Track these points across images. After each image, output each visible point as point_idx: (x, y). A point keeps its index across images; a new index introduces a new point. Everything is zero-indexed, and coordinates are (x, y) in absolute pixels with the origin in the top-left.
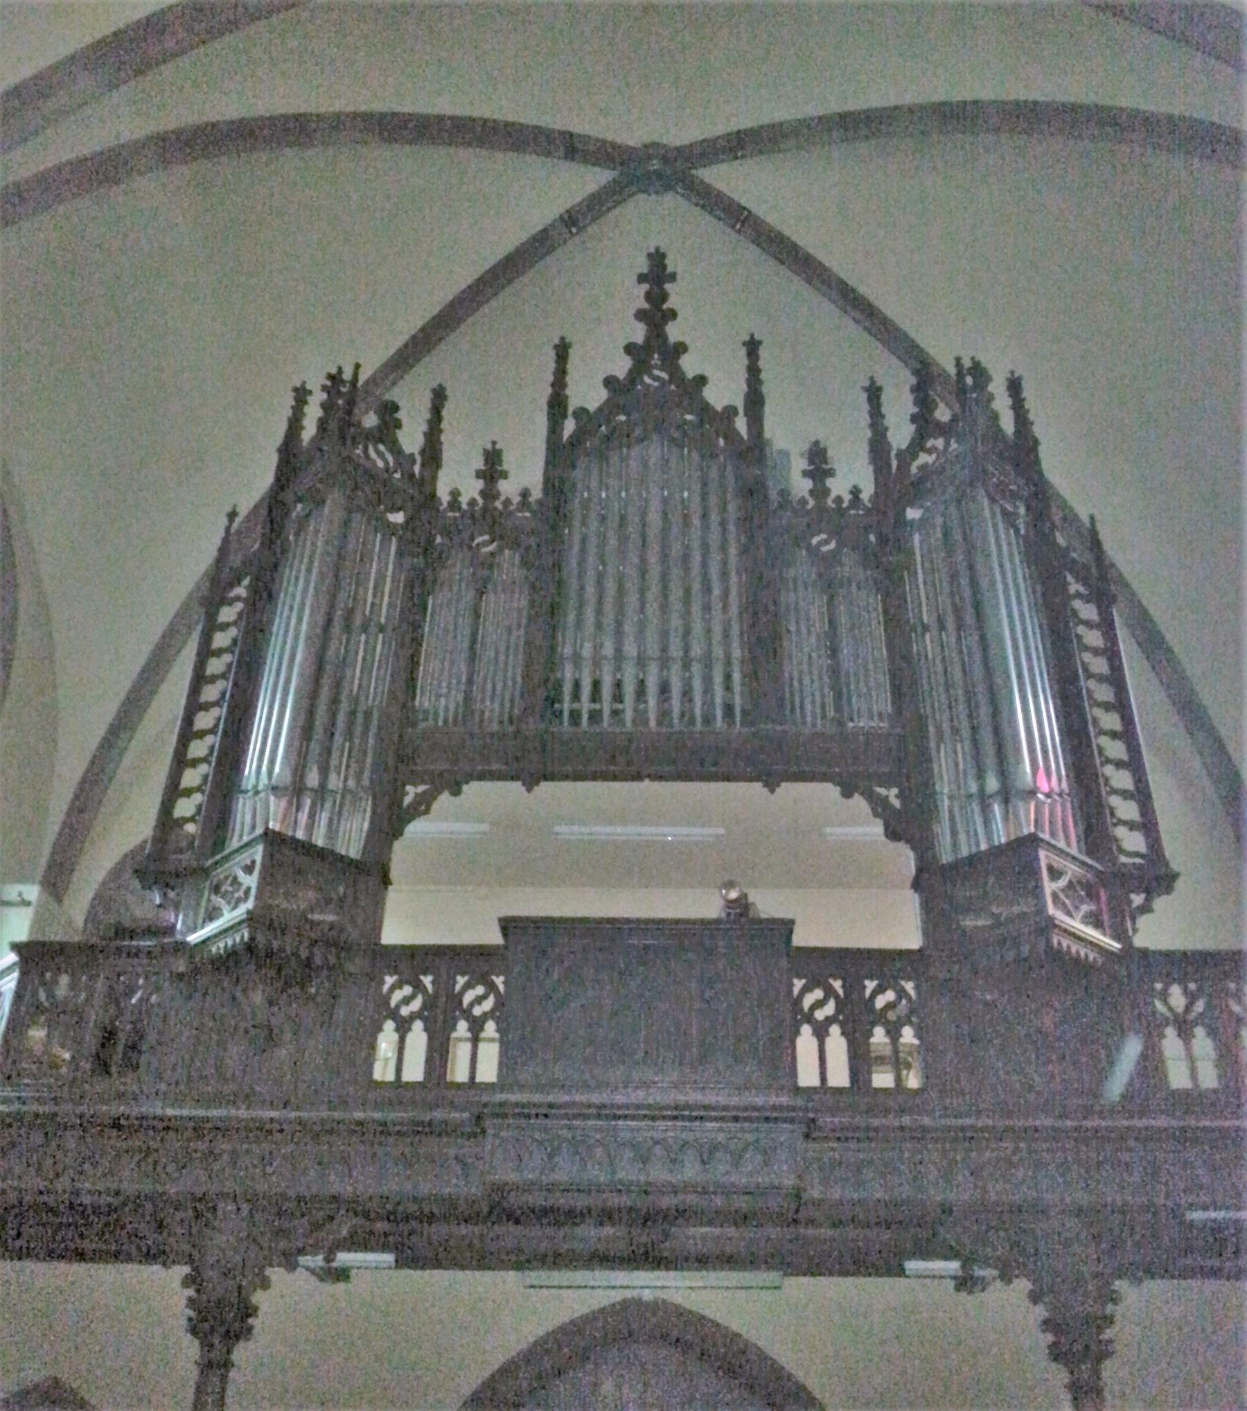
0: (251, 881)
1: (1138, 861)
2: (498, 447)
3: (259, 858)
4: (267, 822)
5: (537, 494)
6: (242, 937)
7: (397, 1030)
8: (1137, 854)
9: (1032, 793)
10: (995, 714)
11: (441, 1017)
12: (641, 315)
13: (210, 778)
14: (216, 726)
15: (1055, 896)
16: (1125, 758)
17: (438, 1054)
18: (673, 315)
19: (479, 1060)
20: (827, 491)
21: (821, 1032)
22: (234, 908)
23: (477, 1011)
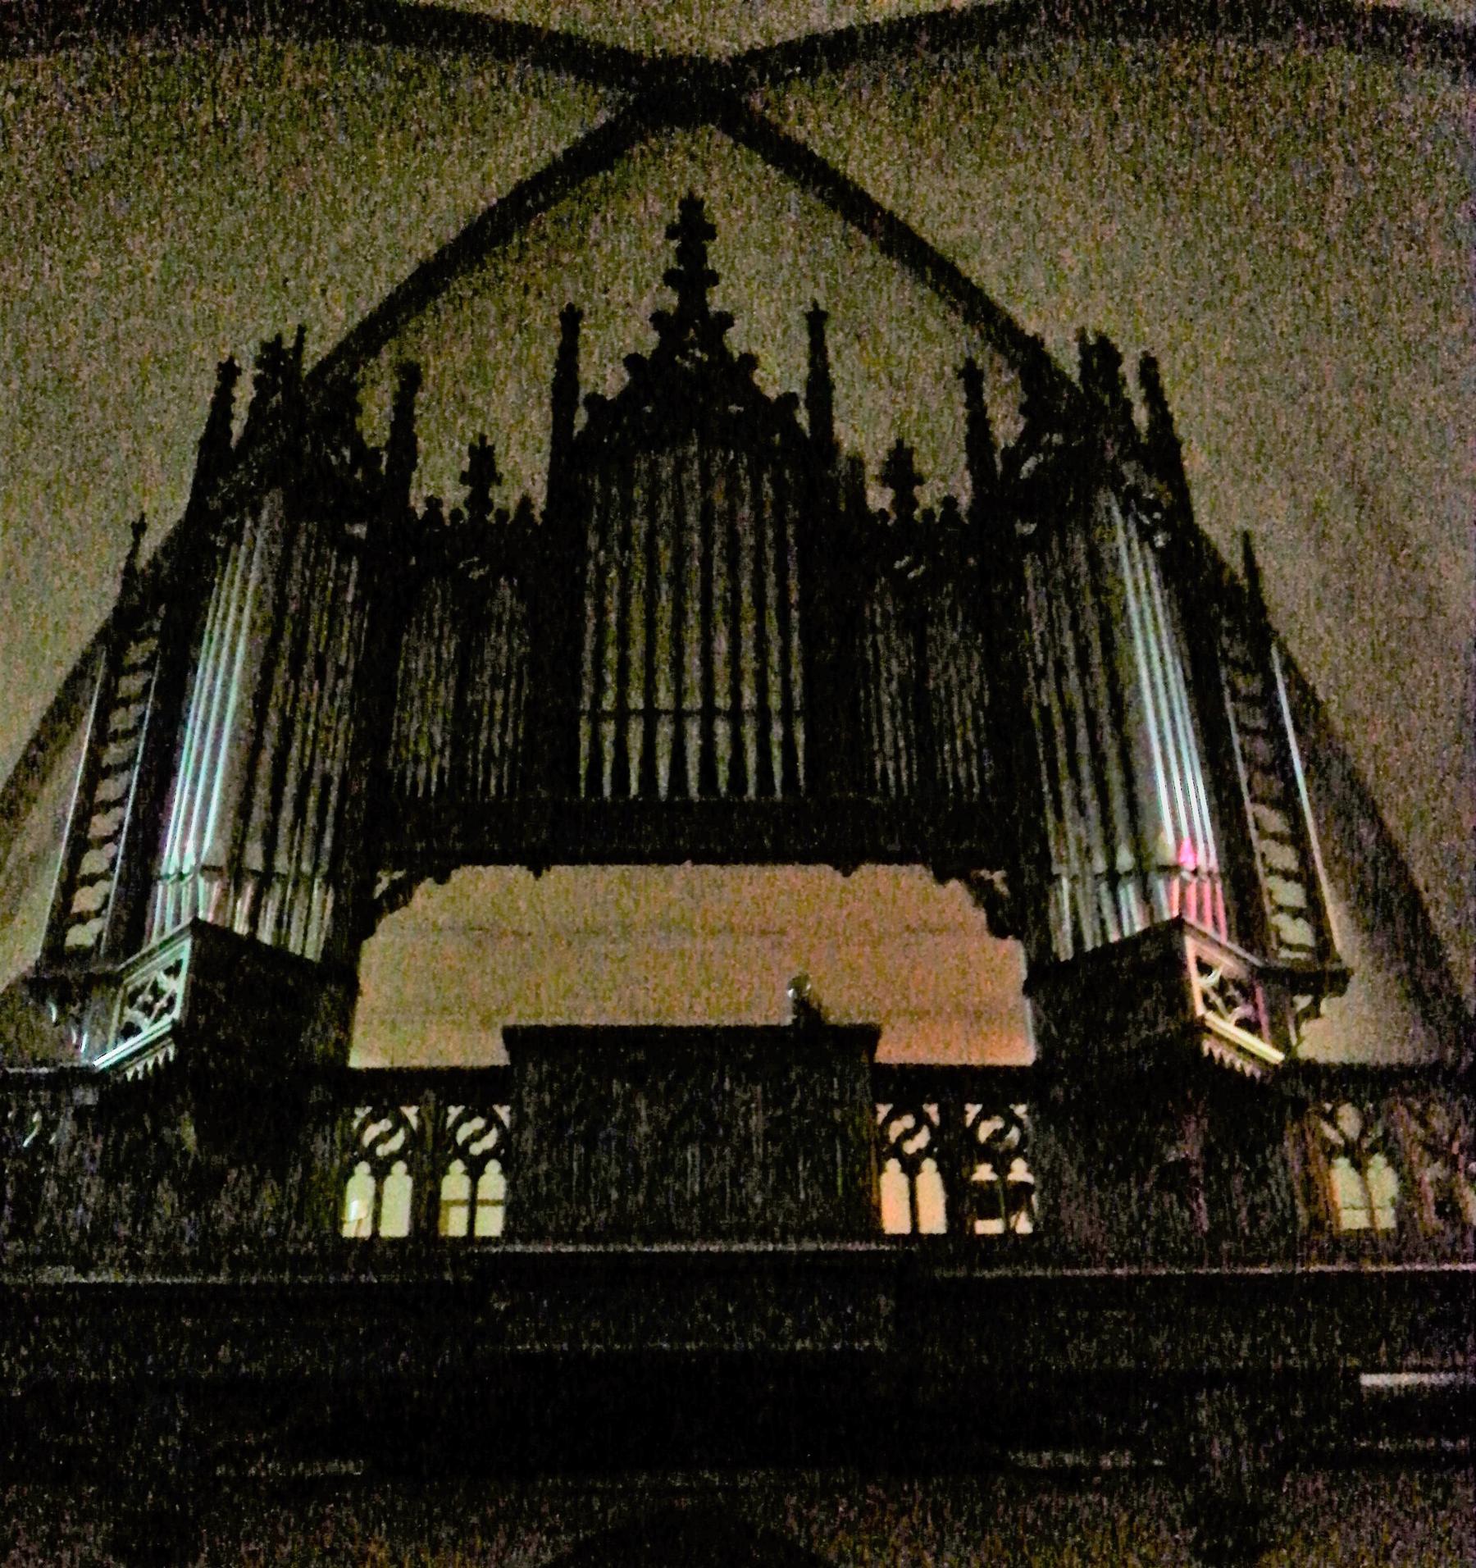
0: (176, 986)
1: (1302, 956)
2: (489, 442)
3: (185, 956)
4: (195, 910)
5: (540, 502)
6: (166, 1057)
7: (904, 1170)
8: (1300, 948)
9: (1176, 869)
10: (1130, 781)
11: (429, 1157)
12: (670, 278)
13: (119, 861)
14: (118, 832)
15: (1205, 997)
16: (1287, 831)
17: (427, 1205)
18: (714, 279)
19: (476, 1205)
20: (914, 504)
21: (911, 1167)
22: (156, 1021)
23: (476, 1149)
